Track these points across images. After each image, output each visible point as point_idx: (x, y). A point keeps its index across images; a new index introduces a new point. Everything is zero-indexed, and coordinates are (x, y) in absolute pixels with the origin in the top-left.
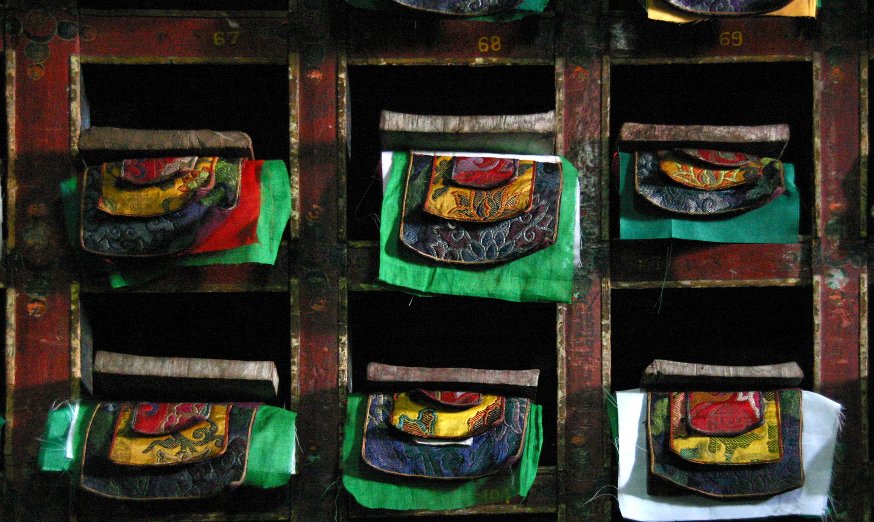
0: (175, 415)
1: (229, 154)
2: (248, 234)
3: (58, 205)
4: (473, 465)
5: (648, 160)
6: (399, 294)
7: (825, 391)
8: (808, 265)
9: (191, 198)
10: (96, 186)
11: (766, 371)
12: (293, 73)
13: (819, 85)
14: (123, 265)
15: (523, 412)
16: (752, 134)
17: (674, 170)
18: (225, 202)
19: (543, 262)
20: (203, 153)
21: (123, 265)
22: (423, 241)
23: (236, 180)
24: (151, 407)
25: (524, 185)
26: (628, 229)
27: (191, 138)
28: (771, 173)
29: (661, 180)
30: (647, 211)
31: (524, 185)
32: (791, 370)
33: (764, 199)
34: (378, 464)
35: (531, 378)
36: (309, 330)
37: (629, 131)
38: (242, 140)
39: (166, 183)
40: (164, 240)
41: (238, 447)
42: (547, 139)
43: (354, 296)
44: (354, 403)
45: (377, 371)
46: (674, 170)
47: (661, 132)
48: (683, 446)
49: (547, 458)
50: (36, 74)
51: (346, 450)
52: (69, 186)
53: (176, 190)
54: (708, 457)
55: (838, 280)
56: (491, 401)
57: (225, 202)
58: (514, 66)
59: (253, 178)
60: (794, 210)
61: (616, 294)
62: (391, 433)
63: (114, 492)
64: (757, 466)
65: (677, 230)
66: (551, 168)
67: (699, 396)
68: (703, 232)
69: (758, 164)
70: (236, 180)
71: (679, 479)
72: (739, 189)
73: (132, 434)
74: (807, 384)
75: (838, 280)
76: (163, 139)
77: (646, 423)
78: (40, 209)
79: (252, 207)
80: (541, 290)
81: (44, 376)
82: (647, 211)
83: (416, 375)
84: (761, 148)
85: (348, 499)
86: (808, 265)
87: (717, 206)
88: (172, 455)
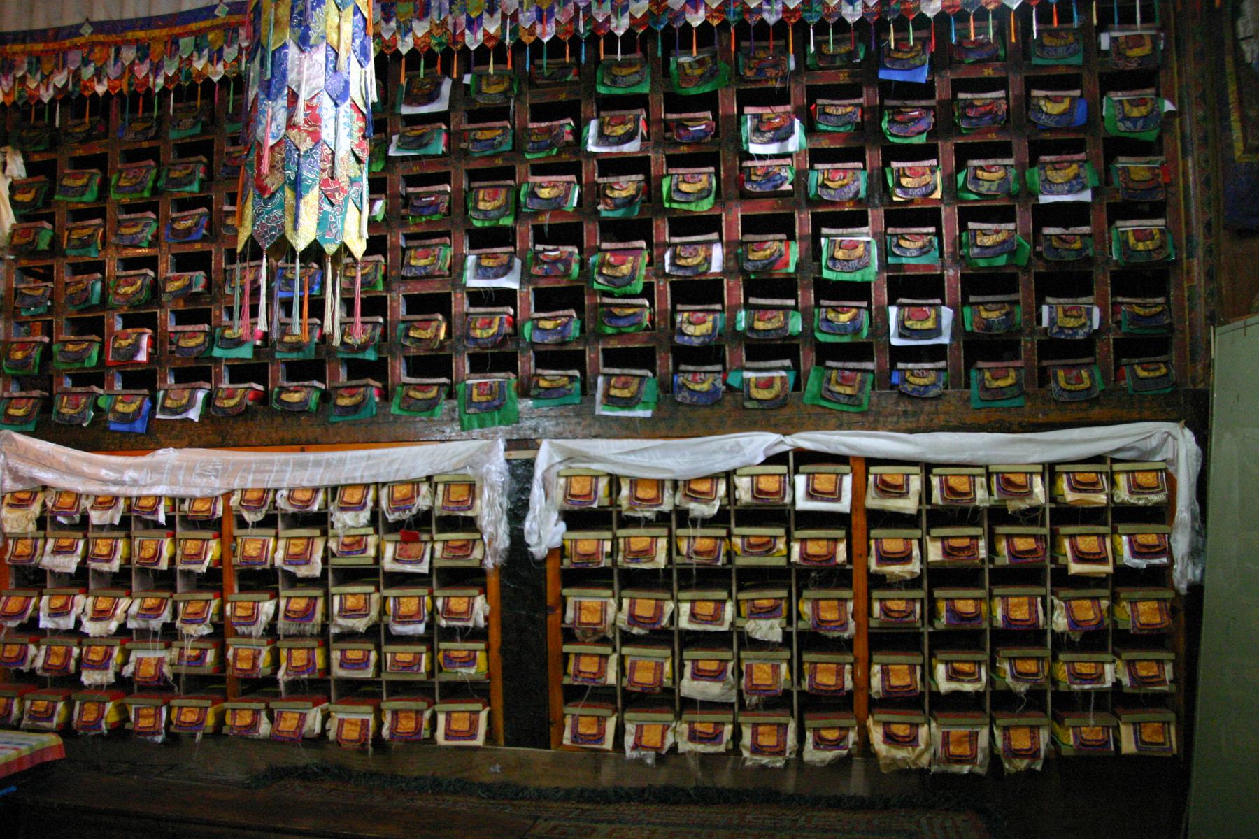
0: (769, 314)
1: (781, 241)
2: (787, 264)
3: (737, 255)
4: (850, 329)
5: (895, 239)
6: (827, 281)
7: (949, 306)
8: (943, 267)
9: (772, 254)
10: (747, 251)
11: (931, 301)
12: (796, 215)
13: (943, 214)
14: (754, 272)
15: (541, 21)
16: (924, 230)
17: (903, 243)
18: (781, 256)
19: (867, 270)
20: (774, 240)
21: (754, 272)
22: (834, 265)
23: (783, 249)
24: (762, 312)
25: (861, 249)
26: (891, 260)
27: (771, 237)
28: (930, 242)
29: (899, 246)
30: (895, 255)
31: (861, 249)
32: (938, 301)
33: (929, 251)
34: (824, 329)
35: (865, 304)
36: (804, 288)
37: (890, 230)
38: (783, 236)
39: (765, 250)
40: (764, 267)
41: (786, 324)
42: (867, 234)
43: (815, 279)
44: (816, 311)
45: (823, 302)
46: (903, 243)
47: (899, 230)
48: (908, 323)
49: (871, 325)
50: (730, 219)
51: (816, 324)
52: (740, 251)
53: (768, 252)
54: (915, 327)
55: (951, 272)
56: (854, 311)
57: (781, 256)
58: (1150, 567)
59: (788, 247)
60: (937, 254)
61: (889, 277)
62: (827, 320)
63: (754, 336)
64: (929, 330)
65: (904, 261)
66: (868, 242)
67: (913, 309)
68: (912, 261)
69: (926, 239)
70: (783, 249)
71: (907, 333)
72: (921, 248)
73: (759, 320)
74: (943, 304)
75: (951, 272)
76: (764, 237)
77: (898, 316)
78: (731, 256)
79: (788, 255)
80: (867, 279)
81: (734, 302)
82: (895, 255)
83: (833, 303)
84: (928, 234)
85: (816, 339)
86: (943, 267)
87: (915, 253)
88: (769, 326)
